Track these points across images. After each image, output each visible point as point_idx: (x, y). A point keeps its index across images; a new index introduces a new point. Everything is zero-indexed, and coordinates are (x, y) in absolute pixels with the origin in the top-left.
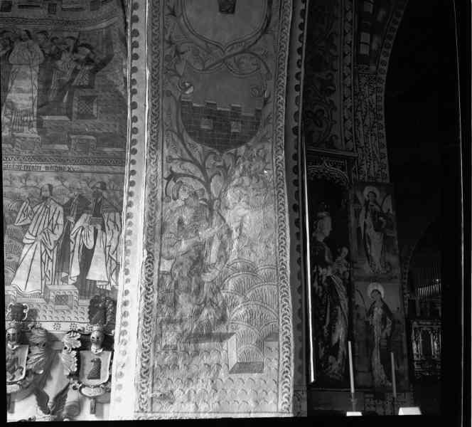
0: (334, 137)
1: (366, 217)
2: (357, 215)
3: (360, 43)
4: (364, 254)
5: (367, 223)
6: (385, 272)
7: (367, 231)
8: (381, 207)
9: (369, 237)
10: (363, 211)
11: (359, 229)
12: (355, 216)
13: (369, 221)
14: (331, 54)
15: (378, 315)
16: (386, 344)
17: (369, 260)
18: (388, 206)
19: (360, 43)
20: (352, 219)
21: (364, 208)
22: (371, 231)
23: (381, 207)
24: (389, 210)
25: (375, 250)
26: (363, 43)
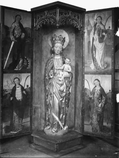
0: (57, 66)
1: (94, 34)
2: (89, 34)
3: (84, 124)
4: (91, 57)
5: (95, 38)
6: (104, 68)
7: (94, 43)
8: (104, 26)
9: (95, 46)
10: (93, 31)
11: (89, 42)
12: (88, 34)
13: (96, 37)
14: (57, 59)
15: (97, 94)
16: (101, 111)
17: (94, 61)
18: (103, 106)
19: (84, 124)
20: (86, 35)
21: (93, 29)
22: (97, 43)
23: (104, 26)
24: (109, 27)
25: (99, 55)
26: (85, 124)
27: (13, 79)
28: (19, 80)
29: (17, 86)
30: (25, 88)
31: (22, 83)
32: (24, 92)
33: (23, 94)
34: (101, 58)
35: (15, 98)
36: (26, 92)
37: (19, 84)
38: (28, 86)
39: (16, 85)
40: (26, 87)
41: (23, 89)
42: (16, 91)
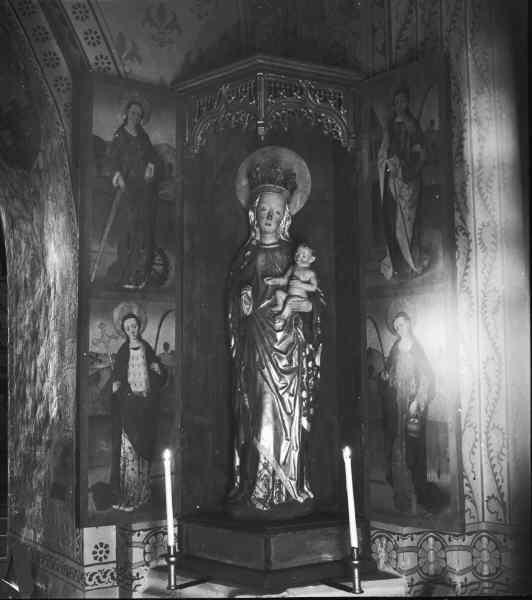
23: (417, 123)
27: (121, 317)
28: (139, 323)
29: (134, 343)
30: (158, 353)
31: (149, 334)
32: (156, 367)
33: (150, 372)
34: (410, 236)
35: (125, 385)
36: (161, 366)
37: (139, 338)
38: (166, 346)
39: (128, 341)
40: (160, 350)
41: (150, 356)
42: (131, 362)
